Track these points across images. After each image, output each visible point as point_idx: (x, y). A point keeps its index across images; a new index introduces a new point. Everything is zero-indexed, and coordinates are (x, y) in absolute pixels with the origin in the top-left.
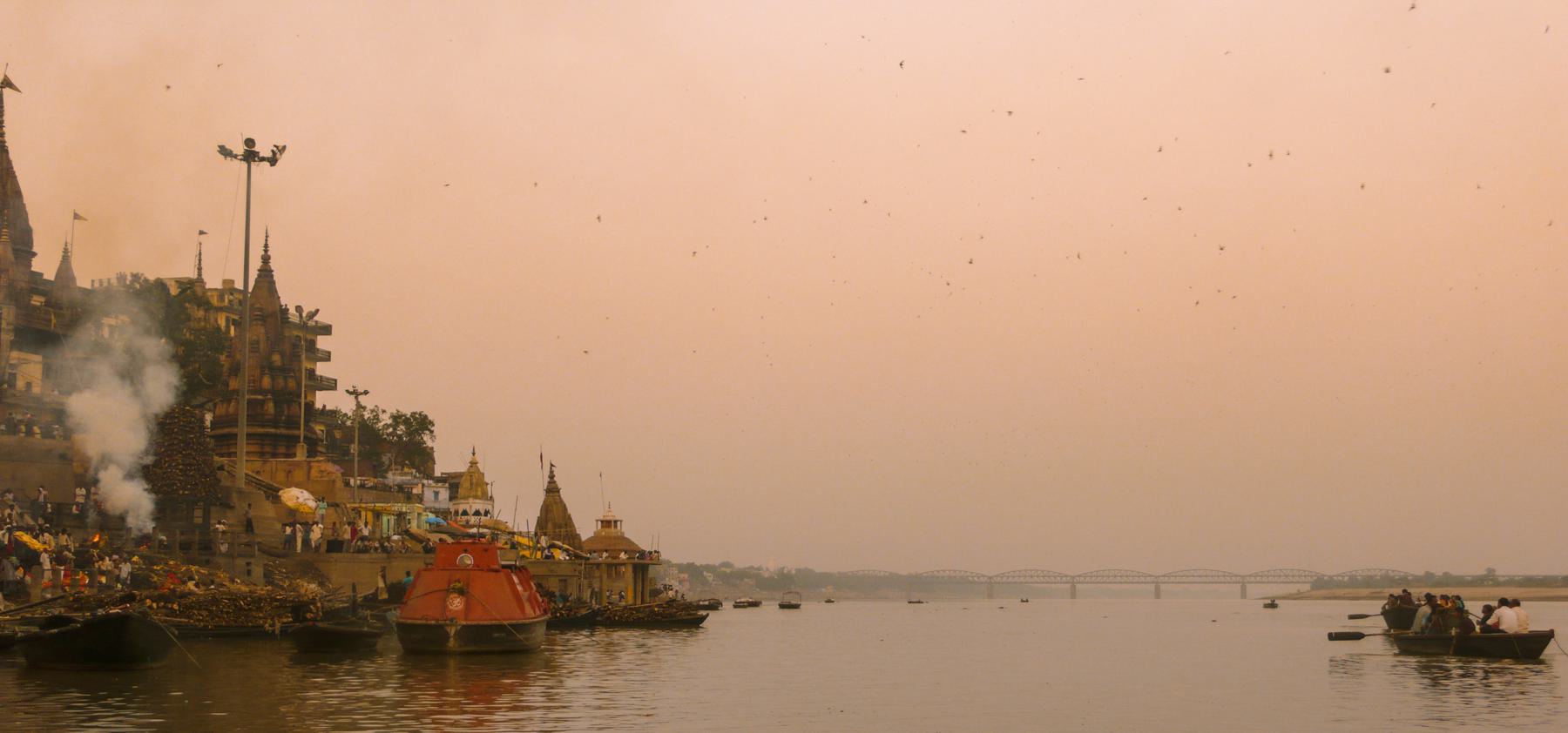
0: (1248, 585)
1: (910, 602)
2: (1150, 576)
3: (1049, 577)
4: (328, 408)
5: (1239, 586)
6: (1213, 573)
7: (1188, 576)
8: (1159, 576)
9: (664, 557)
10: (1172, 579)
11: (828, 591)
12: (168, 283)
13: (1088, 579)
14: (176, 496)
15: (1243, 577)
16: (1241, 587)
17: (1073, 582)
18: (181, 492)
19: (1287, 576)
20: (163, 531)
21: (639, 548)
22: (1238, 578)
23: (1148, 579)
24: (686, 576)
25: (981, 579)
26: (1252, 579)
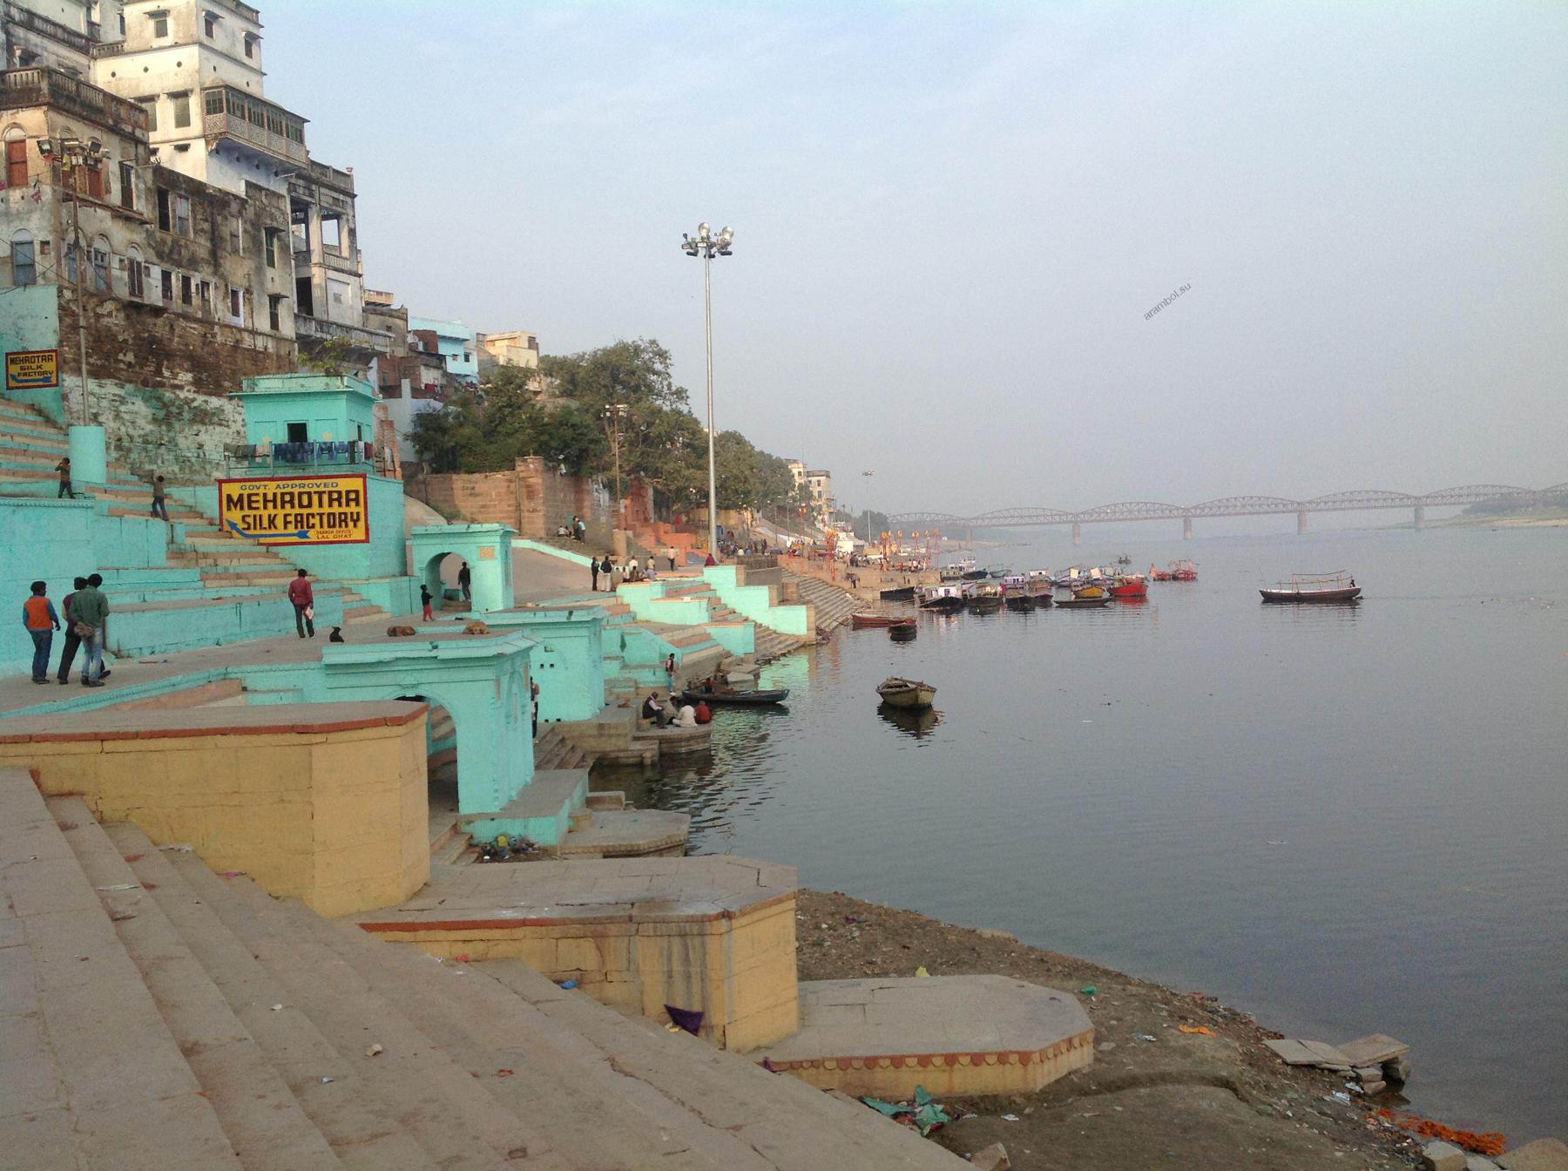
5: (1295, 515)
16: (1299, 516)
25: (1175, 512)
26: (1087, 517)
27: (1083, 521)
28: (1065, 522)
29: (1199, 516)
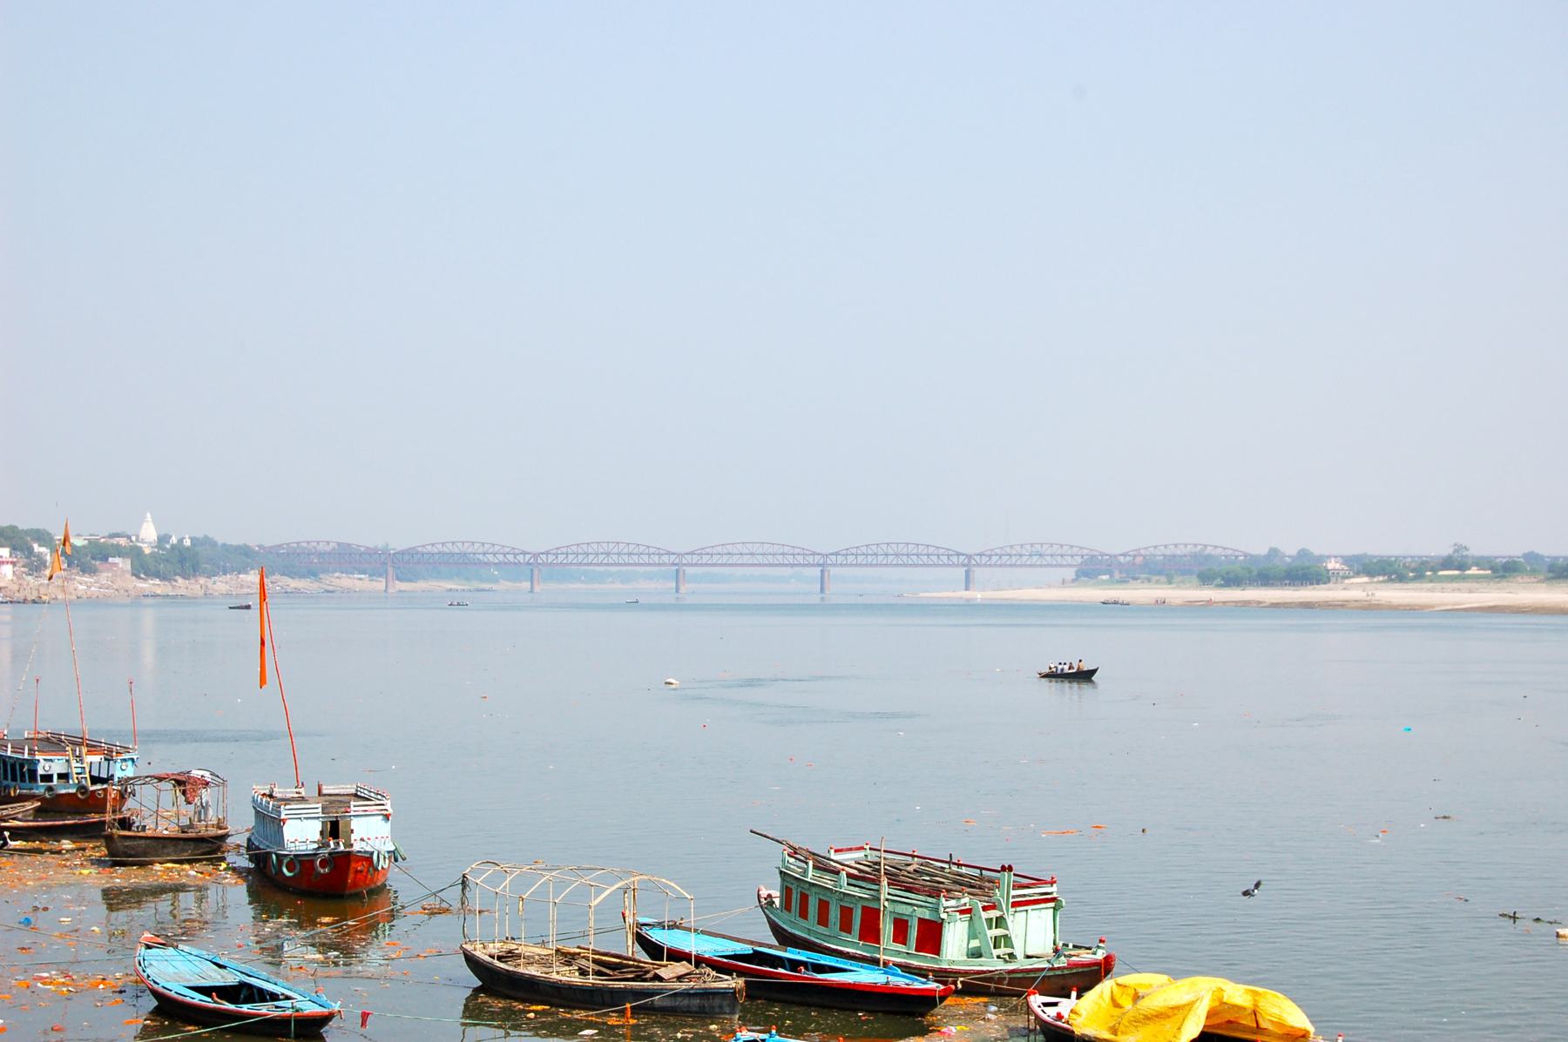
0: (833, 570)
8: (682, 555)
15: (969, 557)
16: (966, 571)
19: (608, 554)
25: (955, 559)
27: (978, 565)
28: (954, 565)
29: (985, 565)
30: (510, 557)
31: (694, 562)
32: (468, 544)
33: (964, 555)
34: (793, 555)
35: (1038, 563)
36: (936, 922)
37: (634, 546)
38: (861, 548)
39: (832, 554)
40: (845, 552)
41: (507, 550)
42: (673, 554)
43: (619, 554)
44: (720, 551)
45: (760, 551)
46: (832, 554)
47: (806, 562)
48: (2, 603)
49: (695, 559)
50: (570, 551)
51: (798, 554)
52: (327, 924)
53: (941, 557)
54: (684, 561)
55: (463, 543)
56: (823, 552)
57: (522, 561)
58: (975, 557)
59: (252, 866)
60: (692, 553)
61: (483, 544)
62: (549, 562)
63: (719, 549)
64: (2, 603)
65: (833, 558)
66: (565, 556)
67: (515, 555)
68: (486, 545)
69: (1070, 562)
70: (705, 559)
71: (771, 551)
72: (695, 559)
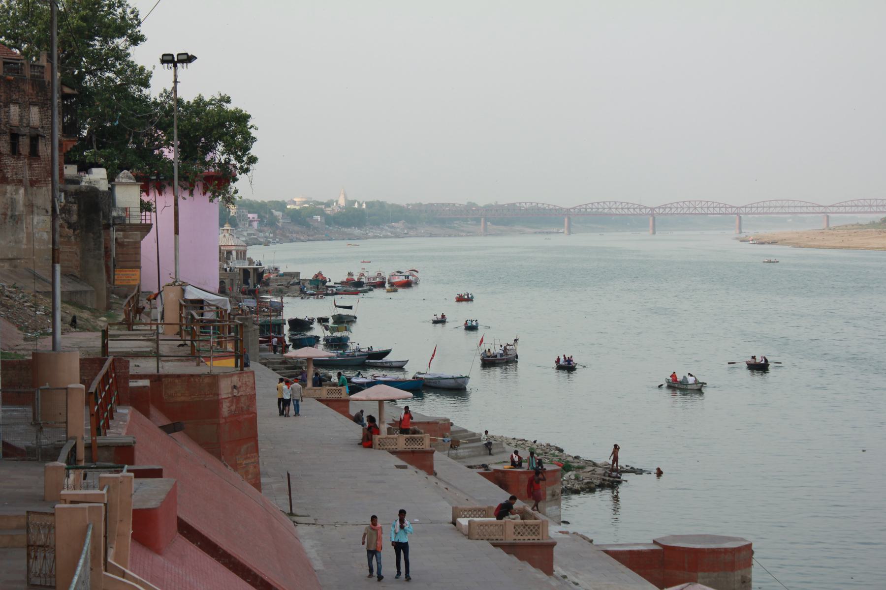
1: (363, 262)
2: (819, 206)
3: (628, 209)
4: (499, 203)
6: (803, 204)
7: (858, 206)
8: (740, 208)
9: (207, 99)
10: (841, 209)
11: (399, 226)
12: (249, 270)
13: (754, 210)
14: (183, 128)
17: (652, 215)
18: (25, 46)
19: (870, 206)
20: (93, 192)
21: (398, 457)
22: (821, 208)
23: (817, 209)
24: (256, 216)
25: (643, 210)
30: (638, 210)
31: (660, 212)
32: (698, 202)
33: (649, 208)
34: (807, 207)
35: (869, 211)
36: (384, 357)
37: (711, 203)
38: (674, 204)
39: (743, 207)
40: (750, 206)
41: (721, 205)
42: (822, 206)
43: (622, 209)
44: (762, 205)
45: (793, 205)
46: (743, 207)
47: (814, 211)
48: (11, 452)
49: (835, 209)
50: (672, 206)
51: (810, 207)
52: (104, 321)
53: (636, 210)
54: (828, 211)
55: (610, 202)
56: (737, 206)
57: (644, 213)
58: (656, 209)
59: (223, 162)
60: (832, 206)
61: (622, 203)
62: (647, 212)
63: (850, 203)
64: (11, 452)
65: (743, 209)
66: (756, 208)
67: (726, 208)
68: (703, 202)
69: (882, 210)
70: (841, 209)
71: (799, 205)
72: (835, 209)
